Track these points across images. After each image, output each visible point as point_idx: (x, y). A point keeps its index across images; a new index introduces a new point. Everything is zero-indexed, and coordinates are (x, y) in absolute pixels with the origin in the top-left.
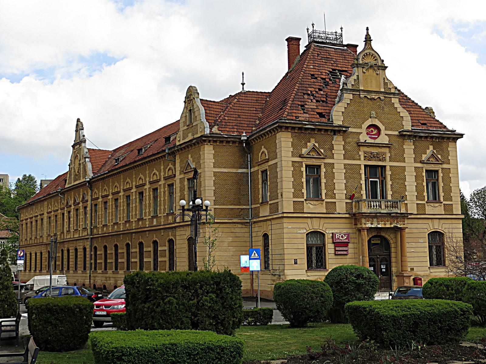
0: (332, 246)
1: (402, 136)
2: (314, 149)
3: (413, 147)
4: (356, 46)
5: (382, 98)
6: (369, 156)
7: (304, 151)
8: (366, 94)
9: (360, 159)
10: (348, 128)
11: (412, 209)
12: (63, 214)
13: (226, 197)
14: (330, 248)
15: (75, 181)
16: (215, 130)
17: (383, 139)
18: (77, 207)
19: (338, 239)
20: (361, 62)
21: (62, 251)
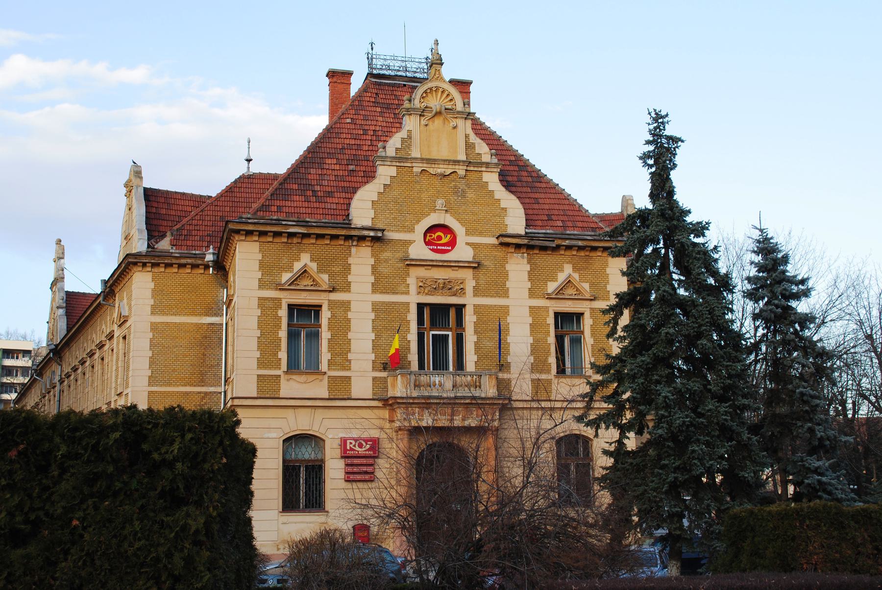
0: (341, 464)
3: (528, 268)
4: (349, 74)
8: (425, 165)
9: (407, 293)
13: (174, 371)
14: (334, 470)
19: (351, 449)
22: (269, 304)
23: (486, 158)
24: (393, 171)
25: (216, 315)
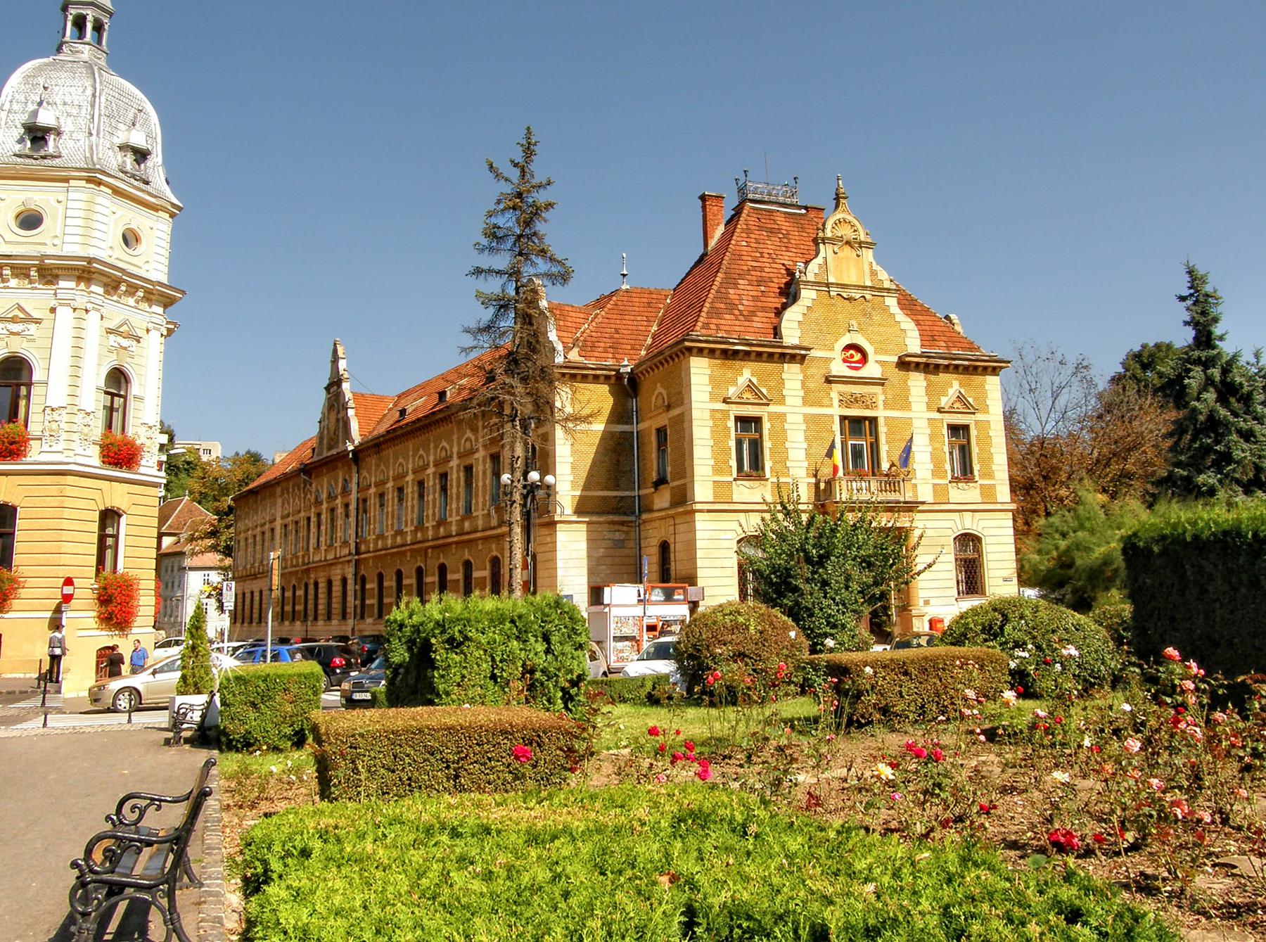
1: (904, 364)
2: (750, 387)
5: (868, 297)
6: (847, 401)
7: (732, 391)
10: (809, 349)
11: (925, 493)
12: (309, 519)
15: (329, 449)
16: (574, 356)
17: (872, 370)
18: (332, 505)
20: (829, 234)
21: (306, 585)
22: (719, 415)
23: (887, 285)
24: (813, 294)
25: (626, 423)
